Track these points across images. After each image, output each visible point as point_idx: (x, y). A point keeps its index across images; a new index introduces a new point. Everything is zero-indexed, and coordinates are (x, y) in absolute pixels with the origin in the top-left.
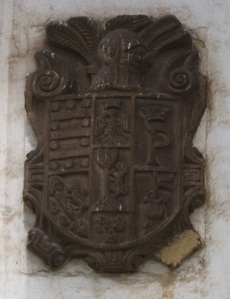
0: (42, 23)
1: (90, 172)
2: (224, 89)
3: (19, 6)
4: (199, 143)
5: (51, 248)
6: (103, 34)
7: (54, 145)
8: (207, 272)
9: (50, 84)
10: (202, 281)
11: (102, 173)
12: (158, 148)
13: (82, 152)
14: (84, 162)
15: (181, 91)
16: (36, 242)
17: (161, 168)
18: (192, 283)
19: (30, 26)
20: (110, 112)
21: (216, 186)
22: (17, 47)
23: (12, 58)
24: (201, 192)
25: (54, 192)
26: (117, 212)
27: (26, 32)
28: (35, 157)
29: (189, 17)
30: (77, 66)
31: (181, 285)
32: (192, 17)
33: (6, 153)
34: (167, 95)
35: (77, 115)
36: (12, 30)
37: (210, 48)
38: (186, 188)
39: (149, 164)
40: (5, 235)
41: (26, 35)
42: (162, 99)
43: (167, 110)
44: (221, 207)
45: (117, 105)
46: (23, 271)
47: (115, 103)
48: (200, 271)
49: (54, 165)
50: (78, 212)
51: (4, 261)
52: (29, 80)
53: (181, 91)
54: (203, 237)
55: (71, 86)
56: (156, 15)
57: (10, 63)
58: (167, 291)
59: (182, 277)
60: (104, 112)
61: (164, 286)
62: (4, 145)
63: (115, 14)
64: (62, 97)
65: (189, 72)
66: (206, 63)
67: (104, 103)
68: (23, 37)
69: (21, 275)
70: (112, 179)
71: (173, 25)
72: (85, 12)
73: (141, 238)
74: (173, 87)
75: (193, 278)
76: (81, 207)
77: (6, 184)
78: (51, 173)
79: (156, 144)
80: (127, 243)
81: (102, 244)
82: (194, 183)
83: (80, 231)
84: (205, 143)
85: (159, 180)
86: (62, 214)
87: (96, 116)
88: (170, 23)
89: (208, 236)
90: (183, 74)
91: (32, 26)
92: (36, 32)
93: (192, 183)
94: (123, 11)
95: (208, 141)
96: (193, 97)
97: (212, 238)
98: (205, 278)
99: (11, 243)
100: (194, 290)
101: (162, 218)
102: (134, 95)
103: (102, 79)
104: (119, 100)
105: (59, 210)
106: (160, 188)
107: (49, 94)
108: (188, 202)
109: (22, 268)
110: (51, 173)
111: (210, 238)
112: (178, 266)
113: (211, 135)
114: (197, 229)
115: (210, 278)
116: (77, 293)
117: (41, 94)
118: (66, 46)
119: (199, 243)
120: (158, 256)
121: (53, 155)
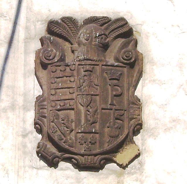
0: (44, 19)
1: (75, 109)
2: (152, 61)
3: (30, 9)
4: (137, 93)
5: (53, 152)
6: (82, 26)
7: (53, 92)
8: (143, 169)
9: (50, 56)
10: (141, 174)
11: (82, 109)
12: (115, 96)
13: (70, 97)
14: (72, 102)
15: (128, 62)
16: (42, 150)
17: (117, 107)
18: (135, 175)
19: (37, 21)
20: (86, 73)
21: (148, 118)
22: (29, 34)
23: (26, 40)
24: (140, 122)
25: (54, 120)
26: (92, 133)
27: (34, 24)
28: (42, 99)
29: (131, 18)
30: (65, 45)
31: (128, 177)
32: (133, 18)
33: (23, 96)
34: (121, 64)
35: (66, 74)
36: (26, 23)
37: (144, 36)
38: (131, 119)
39: (110, 105)
40: (24, 145)
41: (34, 26)
42: (117, 66)
43: (119, 73)
44: (151, 131)
45: (91, 69)
46: (34, 166)
47: (88, 67)
48: (139, 169)
49: (53, 104)
50: (68, 132)
51: (23, 160)
52: (38, 53)
53: (128, 62)
54: (140, 149)
55: (63, 58)
56: (113, 17)
57: (25, 42)
58: (120, 180)
59: (129, 172)
60: (83, 73)
61: (118, 177)
62: (22, 91)
63: (88, 15)
64: (58, 64)
65: (133, 51)
66: (142, 45)
67: (83, 68)
68: (32, 27)
69: (33, 169)
70: (89, 113)
71: (123, 23)
72: (69, 13)
73: (105, 148)
74: (123, 59)
75: (135, 173)
76: (70, 129)
77: (23, 114)
78: (51, 109)
79: (114, 93)
80: (98, 151)
81: (82, 152)
82: (137, 117)
83: (70, 143)
84: (141, 93)
85: (116, 114)
86: (59, 133)
87: (78, 76)
88: (122, 22)
89: (144, 148)
90: (130, 51)
91: (38, 21)
92: (40, 24)
93: (135, 116)
94: (92, 13)
95: (143, 91)
96: (133, 64)
97: (146, 149)
98: (142, 172)
99: (27, 150)
100: (136, 180)
101: (117, 136)
102: (101, 64)
103: (82, 53)
104: (92, 66)
105: (57, 131)
106: (117, 119)
107: (50, 62)
108: (132, 128)
109: (34, 164)
110: (51, 109)
111: (145, 149)
112: (127, 166)
113: (145, 89)
114: (137, 144)
115: (145, 173)
116: (66, 180)
117: (45, 62)
118: (59, 33)
119: (139, 152)
120: (115, 159)
121: (52, 98)
